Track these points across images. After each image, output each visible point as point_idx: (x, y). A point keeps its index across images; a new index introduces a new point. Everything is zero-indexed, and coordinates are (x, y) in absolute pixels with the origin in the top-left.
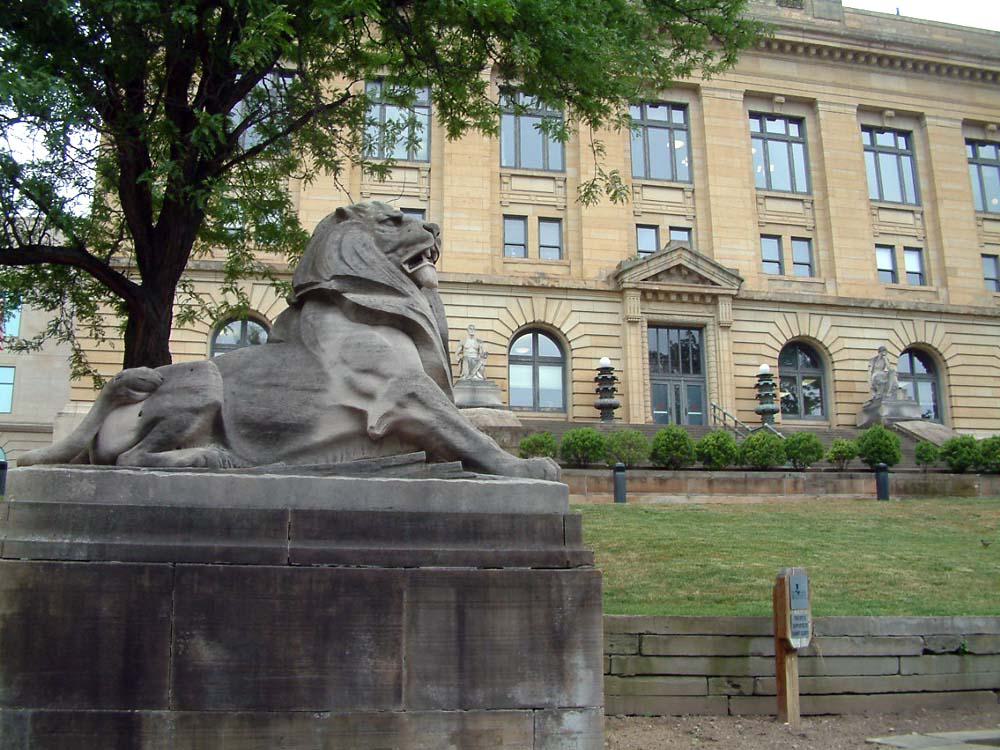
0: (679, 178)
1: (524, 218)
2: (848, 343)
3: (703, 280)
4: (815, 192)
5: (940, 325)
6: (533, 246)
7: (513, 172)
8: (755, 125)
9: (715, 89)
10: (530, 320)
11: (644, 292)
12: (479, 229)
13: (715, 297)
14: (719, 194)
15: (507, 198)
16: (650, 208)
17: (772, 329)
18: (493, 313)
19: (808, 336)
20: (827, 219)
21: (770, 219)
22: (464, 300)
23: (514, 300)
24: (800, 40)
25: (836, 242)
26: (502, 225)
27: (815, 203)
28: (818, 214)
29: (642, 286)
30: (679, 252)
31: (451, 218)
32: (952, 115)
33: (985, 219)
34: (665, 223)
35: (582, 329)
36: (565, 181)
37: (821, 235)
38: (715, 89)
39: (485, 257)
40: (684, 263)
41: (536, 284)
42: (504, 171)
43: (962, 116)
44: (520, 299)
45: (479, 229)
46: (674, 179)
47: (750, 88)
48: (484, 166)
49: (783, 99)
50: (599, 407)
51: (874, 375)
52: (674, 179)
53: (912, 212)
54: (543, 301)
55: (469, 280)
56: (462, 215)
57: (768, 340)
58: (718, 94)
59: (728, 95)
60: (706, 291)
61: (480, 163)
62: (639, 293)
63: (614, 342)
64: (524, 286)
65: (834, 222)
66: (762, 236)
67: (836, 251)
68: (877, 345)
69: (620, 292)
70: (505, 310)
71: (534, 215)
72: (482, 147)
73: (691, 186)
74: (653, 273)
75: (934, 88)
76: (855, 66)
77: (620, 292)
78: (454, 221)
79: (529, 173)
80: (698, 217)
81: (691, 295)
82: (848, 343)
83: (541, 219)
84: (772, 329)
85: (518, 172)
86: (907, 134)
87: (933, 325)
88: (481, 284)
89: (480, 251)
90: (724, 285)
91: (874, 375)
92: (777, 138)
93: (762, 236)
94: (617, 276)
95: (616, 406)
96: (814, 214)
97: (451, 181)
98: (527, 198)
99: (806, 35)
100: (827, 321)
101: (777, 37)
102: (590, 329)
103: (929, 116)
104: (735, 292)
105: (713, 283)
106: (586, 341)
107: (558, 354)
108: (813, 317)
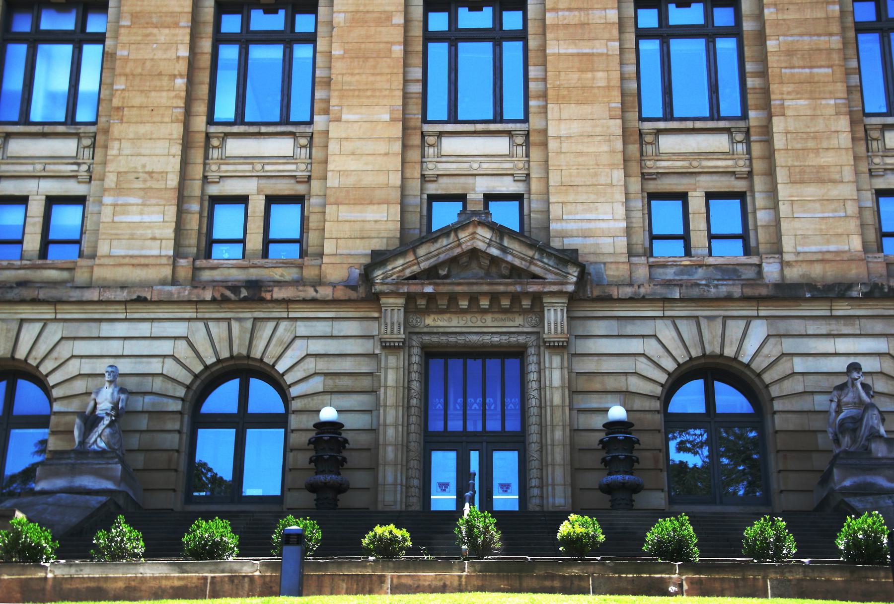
1: (242, 200)
2: (82, 347)
4: (752, 114)
6: (699, 239)
7: (661, 125)
11: (410, 298)
12: (157, 218)
14: (563, 132)
16: (452, 167)
18: (166, 347)
20: (770, 156)
22: (121, 329)
25: (783, 192)
27: (752, 131)
28: (757, 149)
31: (115, 205)
35: (310, 365)
36: (312, 137)
37: (759, 183)
39: (164, 261)
40: (481, 246)
45: (157, 218)
48: (172, 122)
50: (312, 488)
51: (841, 416)
53: (728, 131)
56: (132, 200)
57: (644, 367)
60: (502, 288)
61: (167, 119)
63: (366, 383)
65: (780, 159)
67: (784, 209)
68: (840, 365)
69: (373, 299)
71: (259, 193)
72: (172, 94)
74: (424, 265)
77: (373, 299)
78: (118, 208)
79: (689, 125)
80: (533, 175)
81: (495, 297)
83: (710, 196)
84: (652, 348)
89: (156, 252)
91: (841, 416)
96: (749, 152)
97: (120, 149)
102: (323, 365)
105: (535, 276)
106: (316, 384)
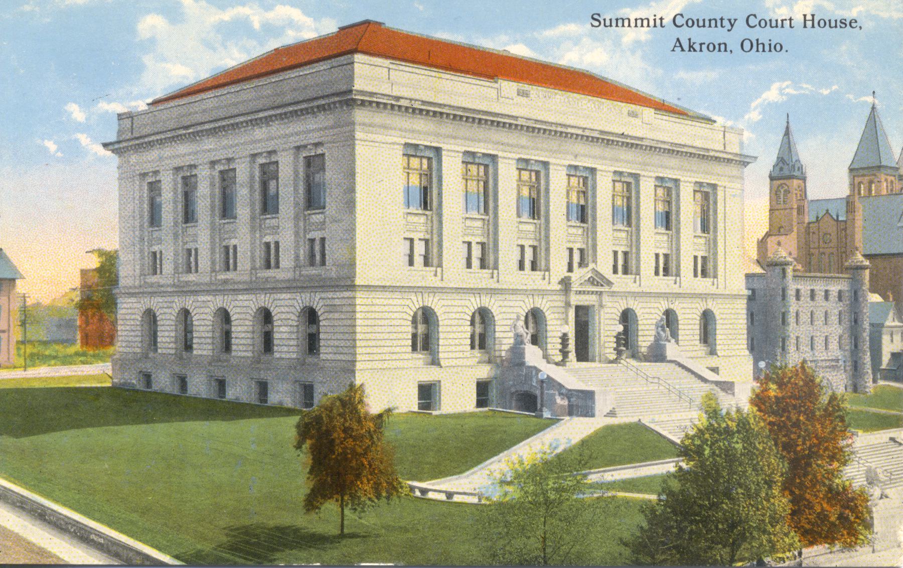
76: (400, 113)
86: (629, 184)
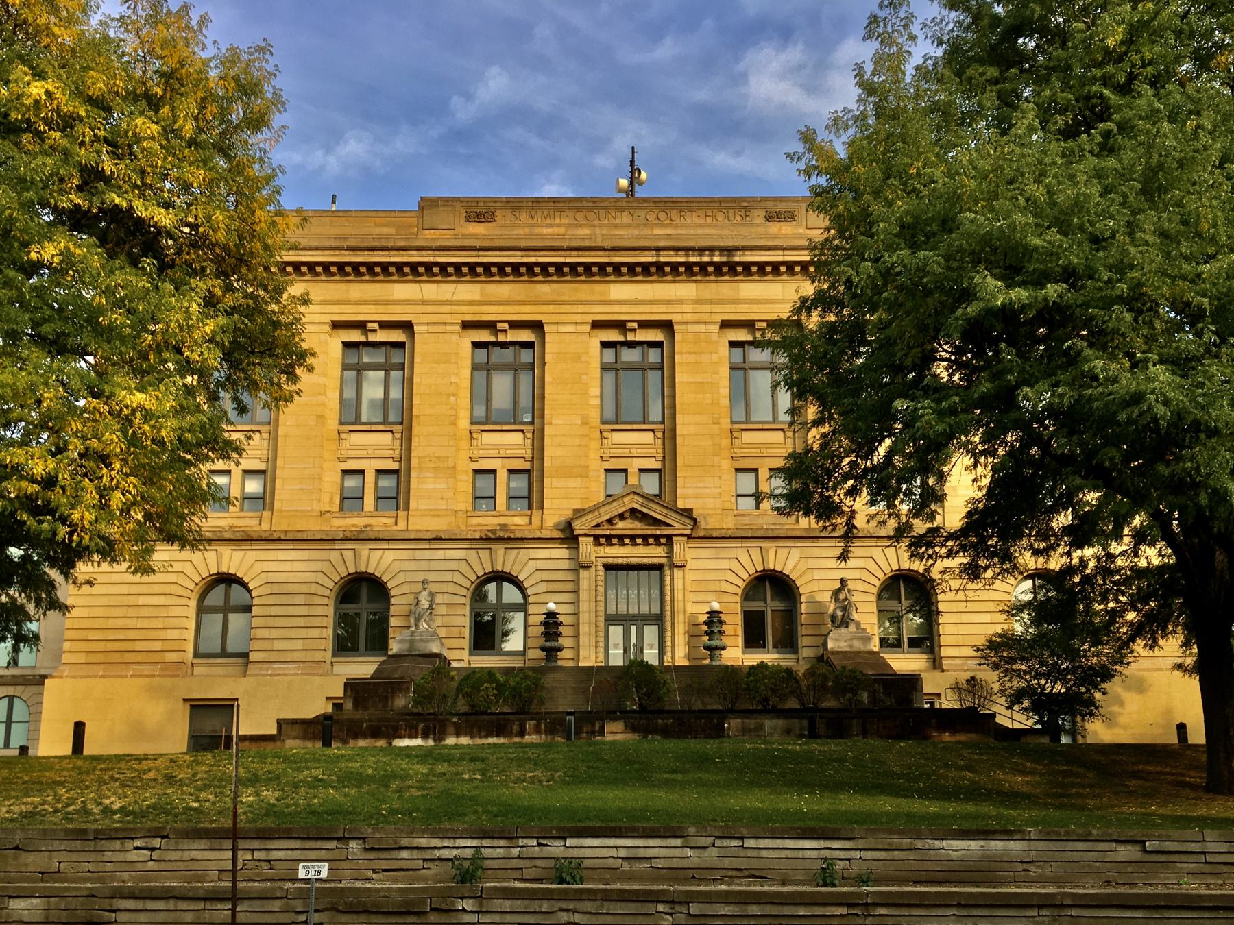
0: (651, 419)
3: (656, 522)
5: (793, 550)
7: (744, 426)
8: (609, 355)
9: (687, 323)
10: (489, 570)
11: (596, 538)
12: (443, 486)
13: (669, 538)
14: (685, 433)
15: (476, 453)
17: (735, 565)
18: (454, 566)
19: (235, 575)
21: (745, 452)
23: (474, 551)
24: (780, 259)
26: (339, 481)
29: (592, 533)
30: (631, 496)
32: (578, 318)
33: (482, 431)
34: (634, 465)
35: (539, 576)
38: (687, 323)
41: (492, 537)
42: (474, 427)
43: (328, 319)
44: (479, 551)
46: (774, 421)
47: (726, 317)
49: (635, 325)
52: (774, 421)
54: (503, 550)
55: (429, 536)
58: (691, 328)
59: (702, 328)
62: (592, 539)
64: (481, 539)
66: (737, 470)
68: (420, 577)
70: (328, 563)
71: (503, 468)
73: (662, 426)
75: (544, 289)
82: (817, 575)
83: (510, 471)
85: (487, 427)
87: (786, 550)
88: (441, 539)
89: (445, 507)
90: (677, 525)
92: (631, 367)
93: (737, 470)
94: (568, 526)
95: (560, 649)
98: (365, 452)
99: (786, 252)
100: (795, 554)
101: (737, 259)
102: (546, 576)
103: (548, 324)
104: (688, 532)
106: (543, 587)
107: (521, 601)
108: (779, 550)
